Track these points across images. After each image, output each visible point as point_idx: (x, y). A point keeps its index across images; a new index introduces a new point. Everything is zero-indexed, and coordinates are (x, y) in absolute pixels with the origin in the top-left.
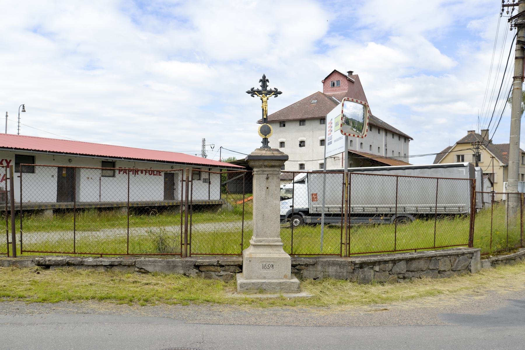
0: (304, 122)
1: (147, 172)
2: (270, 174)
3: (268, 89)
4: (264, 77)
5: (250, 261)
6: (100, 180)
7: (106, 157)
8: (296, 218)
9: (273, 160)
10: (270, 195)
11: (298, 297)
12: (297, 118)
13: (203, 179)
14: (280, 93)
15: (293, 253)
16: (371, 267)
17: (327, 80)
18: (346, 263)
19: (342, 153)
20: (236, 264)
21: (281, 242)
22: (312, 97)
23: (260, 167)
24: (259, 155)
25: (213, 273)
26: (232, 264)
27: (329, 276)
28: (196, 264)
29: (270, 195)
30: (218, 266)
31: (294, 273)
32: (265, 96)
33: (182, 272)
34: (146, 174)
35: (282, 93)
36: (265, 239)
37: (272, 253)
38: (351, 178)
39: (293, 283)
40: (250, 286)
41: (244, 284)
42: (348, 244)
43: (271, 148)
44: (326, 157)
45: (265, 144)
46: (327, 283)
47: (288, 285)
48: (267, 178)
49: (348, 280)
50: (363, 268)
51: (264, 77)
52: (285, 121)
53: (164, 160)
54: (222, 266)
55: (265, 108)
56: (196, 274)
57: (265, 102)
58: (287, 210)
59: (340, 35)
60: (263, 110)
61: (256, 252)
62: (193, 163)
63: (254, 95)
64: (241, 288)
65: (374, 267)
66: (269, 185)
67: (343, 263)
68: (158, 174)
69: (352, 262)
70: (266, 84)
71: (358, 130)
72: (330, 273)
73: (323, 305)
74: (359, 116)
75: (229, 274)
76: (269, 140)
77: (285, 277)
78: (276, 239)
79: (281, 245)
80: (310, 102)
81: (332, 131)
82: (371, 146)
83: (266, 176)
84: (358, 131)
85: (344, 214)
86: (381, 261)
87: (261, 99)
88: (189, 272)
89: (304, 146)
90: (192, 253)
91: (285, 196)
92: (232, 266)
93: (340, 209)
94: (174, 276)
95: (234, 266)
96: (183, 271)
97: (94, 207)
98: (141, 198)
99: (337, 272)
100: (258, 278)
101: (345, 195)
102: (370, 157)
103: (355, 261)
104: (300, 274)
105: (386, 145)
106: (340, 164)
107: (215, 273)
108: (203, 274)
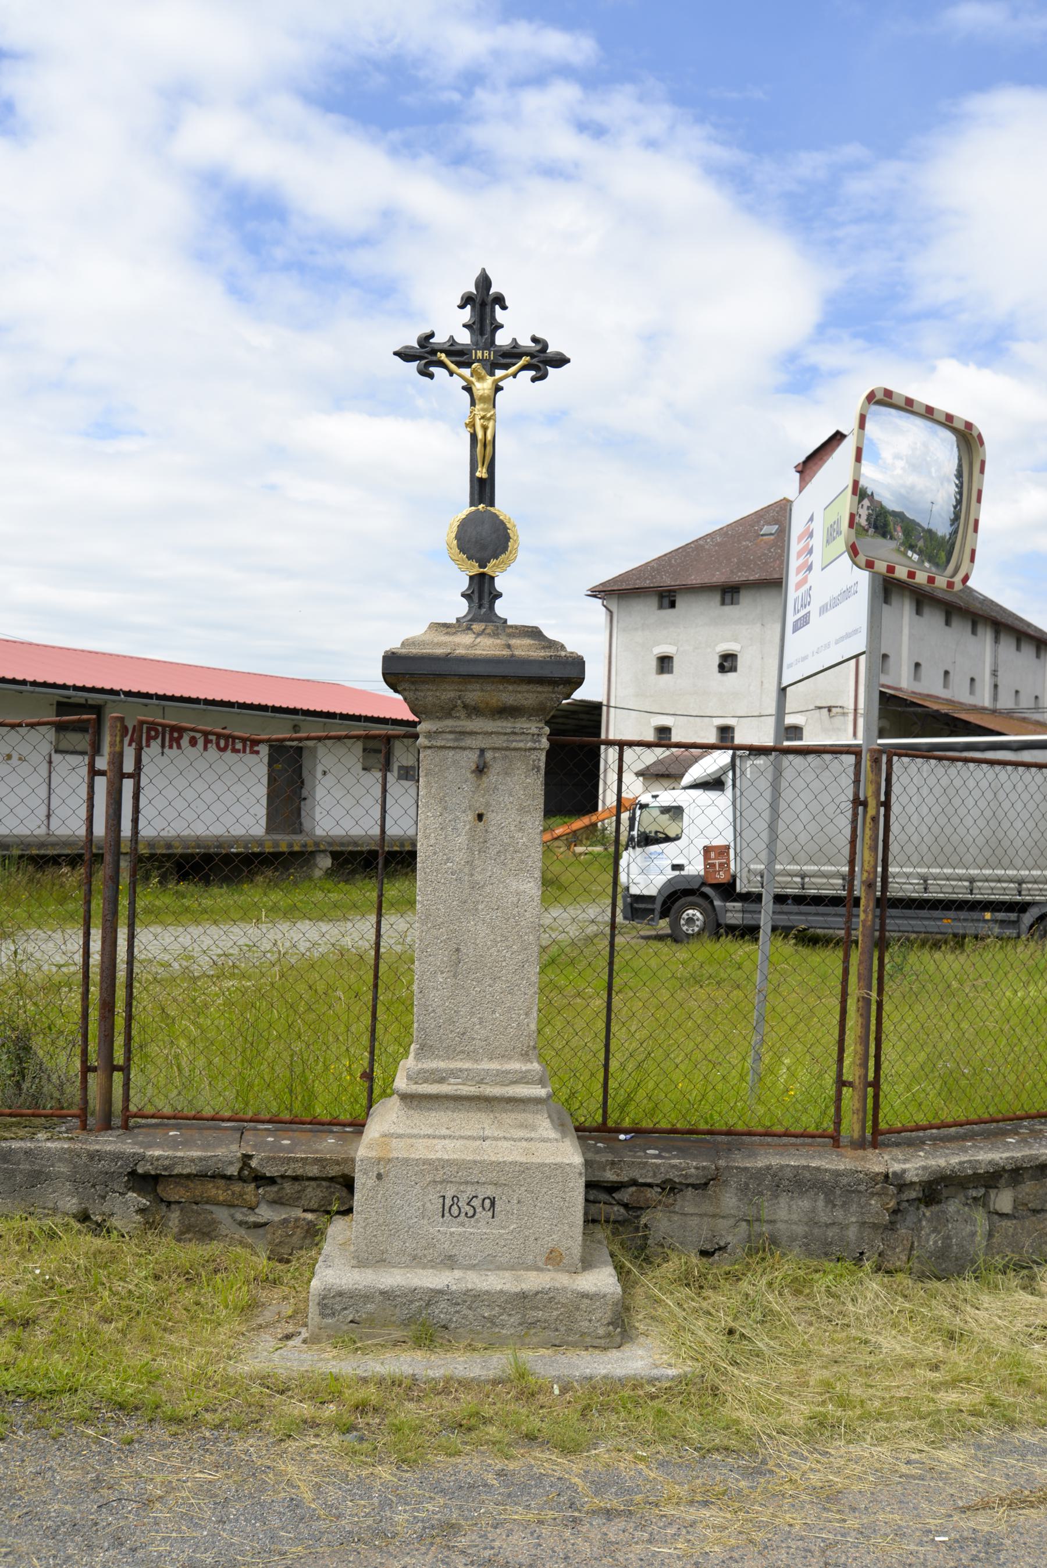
0: (735, 595)
1: (211, 741)
2: (495, 749)
3: (502, 339)
4: (484, 282)
5: (379, 1177)
6: (50, 762)
7: (64, 687)
8: (693, 906)
9: (505, 679)
10: (493, 852)
11: (605, 1377)
12: (714, 580)
13: (400, 768)
14: (560, 361)
15: (610, 1123)
16: (974, 1193)
17: (810, 464)
18: (859, 1182)
19: (857, 656)
20: (332, 1174)
21: (542, 1082)
22: (762, 516)
23: (447, 712)
24: (439, 651)
25: (221, 1214)
26: (314, 1171)
27: (774, 1241)
28: (140, 1171)
29: (493, 852)
30: (245, 1181)
31: (607, 1221)
32: (483, 372)
33: (71, 1204)
34: (205, 748)
35: (567, 361)
36: (459, 1065)
37: (496, 1139)
38: (894, 778)
39: (585, 1295)
40: (370, 1307)
41: (340, 1294)
42: (870, 1085)
43: (509, 623)
44: (784, 684)
45: (480, 606)
46: (764, 1281)
47: (564, 1305)
48: (481, 770)
49: (867, 1265)
50: (939, 1202)
51: (484, 282)
52: (674, 591)
53: (263, 703)
54: (261, 1180)
55: (485, 429)
56: (138, 1217)
57: (483, 399)
58: (660, 880)
59: (856, 336)
60: (474, 437)
61: (415, 1131)
62: (363, 714)
63: (432, 369)
64: (323, 1315)
65: (993, 1193)
66: (488, 805)
67: (845, 1181)
68: (248, 749)
69: (887, 1176)
70: (493, 317)
71: (929, 561)
72: (780, 1226)
73: (733, 1443)
74: (935, 508)
75: (297, 1220)
76: (499, 584)
77: (554, 1259)
78: (516, 1065)
79: (537, 1101)
80: (756, 531)
81: (810, 568)
82: (946, 673)
83: (474, 756)
84: (927, 565)
85: (857, 901)
86: (1022, 1168)
87: (464, 388)
88: (106, 1208)
89: (733, 669)
90: (133, 1108)
91: (656, 832)
92: (313, 1183)
93: (844, 879)
94: (32, 1224)
95: (324, 1183)
96: (74, 1201)
97: (16, 852)
98: (228, 820)
99: (813, 1223)
100: (416, 1261)
101: (865, 855)
102: (945, 707)
103: (904, 1171)
104: (637, 1229)
105: (994, 673)
106: (846, 730)
107: (232, 1211)
108: (175, 1217)
